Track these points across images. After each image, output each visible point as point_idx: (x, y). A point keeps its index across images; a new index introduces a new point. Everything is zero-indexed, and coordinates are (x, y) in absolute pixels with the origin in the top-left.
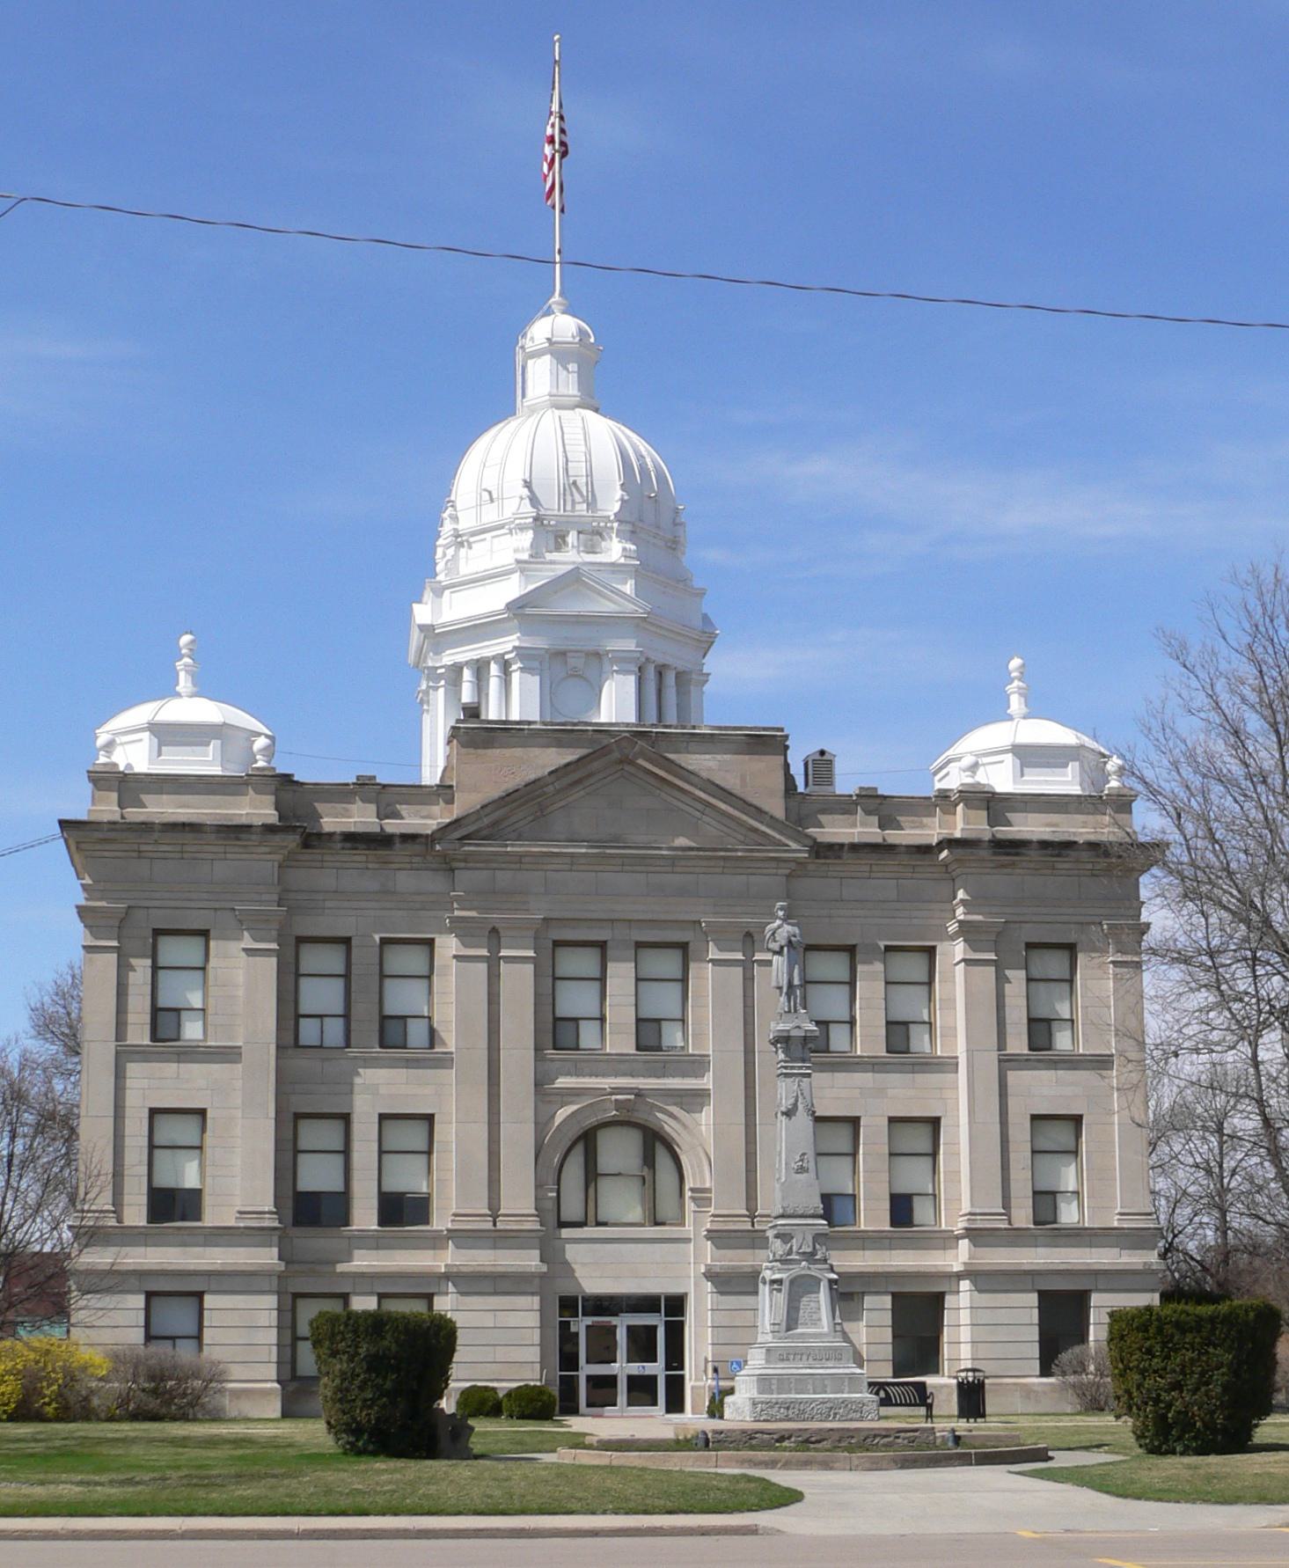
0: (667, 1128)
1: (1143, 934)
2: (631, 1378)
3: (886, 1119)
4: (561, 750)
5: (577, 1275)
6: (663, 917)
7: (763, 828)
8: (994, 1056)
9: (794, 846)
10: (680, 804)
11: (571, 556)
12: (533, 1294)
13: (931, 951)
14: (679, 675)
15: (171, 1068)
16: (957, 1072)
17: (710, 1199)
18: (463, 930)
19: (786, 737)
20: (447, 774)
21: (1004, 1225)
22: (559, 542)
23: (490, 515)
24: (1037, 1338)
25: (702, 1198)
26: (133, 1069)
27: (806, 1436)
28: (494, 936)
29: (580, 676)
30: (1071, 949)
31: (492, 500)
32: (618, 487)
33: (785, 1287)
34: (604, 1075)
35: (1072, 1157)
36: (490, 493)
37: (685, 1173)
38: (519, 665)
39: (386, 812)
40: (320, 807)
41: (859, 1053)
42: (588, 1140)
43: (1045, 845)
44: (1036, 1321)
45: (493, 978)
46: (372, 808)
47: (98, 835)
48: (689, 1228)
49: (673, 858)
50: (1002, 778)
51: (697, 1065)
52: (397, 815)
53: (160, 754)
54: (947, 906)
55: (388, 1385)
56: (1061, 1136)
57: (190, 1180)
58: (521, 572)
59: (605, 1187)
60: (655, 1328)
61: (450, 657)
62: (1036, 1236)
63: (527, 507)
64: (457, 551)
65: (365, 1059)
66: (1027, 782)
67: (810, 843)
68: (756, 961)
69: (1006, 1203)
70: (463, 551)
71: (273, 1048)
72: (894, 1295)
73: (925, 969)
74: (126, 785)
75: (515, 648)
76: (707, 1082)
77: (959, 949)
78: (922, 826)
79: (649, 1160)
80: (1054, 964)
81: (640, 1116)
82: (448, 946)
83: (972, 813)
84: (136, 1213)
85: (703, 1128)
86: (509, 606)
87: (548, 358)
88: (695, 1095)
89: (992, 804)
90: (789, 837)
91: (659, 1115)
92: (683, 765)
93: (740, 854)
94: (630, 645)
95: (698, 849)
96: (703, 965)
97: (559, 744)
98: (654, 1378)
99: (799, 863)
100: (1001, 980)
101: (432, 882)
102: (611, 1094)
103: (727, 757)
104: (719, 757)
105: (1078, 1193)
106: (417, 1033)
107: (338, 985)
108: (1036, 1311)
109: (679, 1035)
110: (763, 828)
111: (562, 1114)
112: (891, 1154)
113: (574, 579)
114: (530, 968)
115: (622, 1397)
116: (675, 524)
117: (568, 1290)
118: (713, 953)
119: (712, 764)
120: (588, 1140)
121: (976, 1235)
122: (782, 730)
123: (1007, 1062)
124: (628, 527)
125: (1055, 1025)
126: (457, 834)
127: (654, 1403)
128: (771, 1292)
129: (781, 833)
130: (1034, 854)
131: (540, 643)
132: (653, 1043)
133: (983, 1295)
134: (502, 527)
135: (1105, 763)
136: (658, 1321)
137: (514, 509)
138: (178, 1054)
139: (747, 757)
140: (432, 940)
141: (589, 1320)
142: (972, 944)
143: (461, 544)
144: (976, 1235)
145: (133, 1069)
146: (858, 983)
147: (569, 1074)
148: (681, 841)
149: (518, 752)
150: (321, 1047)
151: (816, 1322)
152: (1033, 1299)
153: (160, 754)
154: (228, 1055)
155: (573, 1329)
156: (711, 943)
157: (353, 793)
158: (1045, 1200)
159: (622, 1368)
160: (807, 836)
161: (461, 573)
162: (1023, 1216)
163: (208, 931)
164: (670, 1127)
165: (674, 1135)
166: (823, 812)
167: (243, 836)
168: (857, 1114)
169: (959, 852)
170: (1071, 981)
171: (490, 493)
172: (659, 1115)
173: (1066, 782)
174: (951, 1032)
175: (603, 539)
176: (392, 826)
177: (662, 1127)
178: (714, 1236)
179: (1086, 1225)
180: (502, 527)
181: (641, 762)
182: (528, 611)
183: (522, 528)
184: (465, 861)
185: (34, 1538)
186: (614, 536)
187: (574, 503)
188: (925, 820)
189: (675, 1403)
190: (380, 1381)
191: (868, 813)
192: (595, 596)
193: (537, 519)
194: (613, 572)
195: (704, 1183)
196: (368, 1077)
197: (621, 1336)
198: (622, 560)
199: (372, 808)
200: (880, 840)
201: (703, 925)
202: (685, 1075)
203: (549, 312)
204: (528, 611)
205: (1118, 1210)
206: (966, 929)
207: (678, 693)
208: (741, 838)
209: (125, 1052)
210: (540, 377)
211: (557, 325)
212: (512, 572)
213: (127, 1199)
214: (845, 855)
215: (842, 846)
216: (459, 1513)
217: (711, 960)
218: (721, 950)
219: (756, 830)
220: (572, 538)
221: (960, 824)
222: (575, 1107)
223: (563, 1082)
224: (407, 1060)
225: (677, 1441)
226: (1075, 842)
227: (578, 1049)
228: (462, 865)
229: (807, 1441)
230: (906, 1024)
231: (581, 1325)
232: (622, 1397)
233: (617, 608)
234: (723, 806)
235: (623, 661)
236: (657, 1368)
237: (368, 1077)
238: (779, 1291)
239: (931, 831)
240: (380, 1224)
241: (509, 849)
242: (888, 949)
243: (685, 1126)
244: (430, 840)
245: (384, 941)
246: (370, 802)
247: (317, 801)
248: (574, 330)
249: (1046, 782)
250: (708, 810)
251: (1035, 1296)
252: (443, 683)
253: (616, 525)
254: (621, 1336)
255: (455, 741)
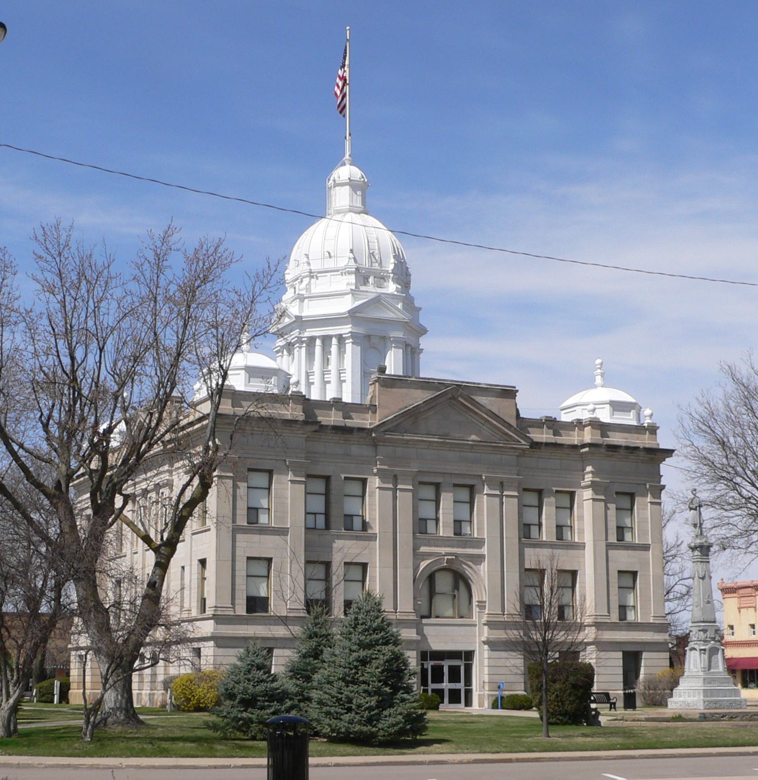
0: (467, 572)
1: (662, 490)
2: (450, 690)
3: (246, 558)
4: (424, 391)
5: (429, 641)
6: (431, 470)
7: (511, 433)
8: (604, 543)
9: (523, 442)
10: (473, 420)
11: (371, 290)
12: (413, 650)
13: (572, 495)
14: (412, 348)
15: (256, 537)
16: (584, 549)
17: (485, 606)
18: (382, 474)
19: (517, 391)
20: (373, 399)
21: (232, 613)
22: (365, 281)
23: (330, 264)
24: (622, 672)
25: (482, 605)
26: (239, 537)
27: (731, 715)
28: (395, 479)
29: (375, 348)
30: (270, 473)
31: (330, 257)
32: (392, 257)
33: (707, 653)
34: (440, 546)
35: (632, 590)
36: (329, 253)
37: (473, 594)
38: (351, 340)
39: (604, 435)
40: (317, 412)
41: (441, 535)
42: (431, 578)
43: (627, 448)
44: (621, 665)
45: (395, 498)
46: (341, 413)
47: (227, 421)
48: (475, 618)
49: (472, 445)
50: (605, 416)
51: (479, 543)
52: (350, 418)
53: (249, 382)
54: (581, 473)
55: (579, 694)
56: (261, 569)
57: (263, 593)
58: (353, 295)
59: (437, 600)
60: (460, 666)
61: (309, 332)
62: (621, 626)
63: (352, 262)
64: (310, 279)
65: (338, 535)
66: (615, 418)
67: (530, 441)
68: (399, 489)
69: (233, 603)
70: (313, 280)
71: (303, 529)
72: (623, 651)
73: (569, 502)
74: (237, 397)
75: (350, 332)
76: (484, 550)
77: (588, 494)
78: (570, 436)
79: (456, 587)
80: (260, 480)
81: (455, 567)
82: (374, 482)
83: (594, 431)
84: (241, 610)
85: (482, 573)
86: (349, 312)
87: (348, 187)
88: (480, 557)
89: (603, 428)
90: (521, 438)
91: (464, 566)
92: (480, 402)
93: (470, 443)
94: (400, 334)
95: (481, 442)
96: (482, 495)
97: (422, 388)
98: (459, 690)
99: (523, 450)
100: (235, 487)
101: (367, 451)
102: (445, 556)
103: (493, 399)
104: (489, 398)
105: (634, 607)
106: (357, 524)
107: (322, 499)
108: (621, 661)
109: (469, 528)
110: (511, 433)
111: (423, 565)
112: (248, 576)
113: (377, 301)
114: (516, 500)
115: (446, 699)
116: (407, 275)
117: (425, 649)
118: (486, 490)
119: (485, 401)
120: (431, 578)
121: (598, 625)
122: (515, 387)
123: (609, 546)
124: (396, 277)
125: (625, 530)
126: (383, 429)
127: (459, 702)
128: (701, 654)
129: (518, 436)
130: (622, 451)
131: (360, 330)
132: (423, 531)
133: (495, 652)
134: (338, 271)
135: (290, 378)
136: (461, 663)
137: (346, 263)
138: (260, 530)
139: (500, 399)
140: (366, 479)
141: (432, 663)
142: (596, 492)
143: (312, 277)
144: (598, 625)
145: (239, 537)
146: (544, 508)
147: (425, 545)
148: (473, 437)
149: (404, 391)
150: (315, 528)
151: (718, 667)
152: (620, 654)
153: (249, 382)
154: (282, 532)
155: (425, 667)
156: (486, 486)
157: (333, 406)
158: (623, 609)
159: (446, 685)
160: (529, 438)
161: (312, 292)
162: (615, 617)
163: (272, 470)
164: (468, 572)
165: (470, 576)
166: (530, 427)
167: (293, 425)
168: (635, 570)
169: (593, 449)
170: (269, 489)
171: (329, 253)
172: (464, 566)
173: (629, 419)
174: (581, 532)
175: (385, 281)
176: (349, 423)
177: (465, 572)
178: (491, 624)
179: (639, 621)
180: (338, 271)
181: (460, 399)
182: (357, 315)
183: (350, 273)
184: (384, 442)
185: (567, 760)
186: (390, 280)
187: (372, 262)
188: (571, 433)
189: (468, 703)
190: (576, 692)
191: (549, 428)
192: (383, 308)
193: (357, 269)
194: (393, 298)
195: (482, 598)
196: (338, 544)
197: (446, 670)
198: (396, 293)
199: (341, 413)
200: (554, 441)
201: (287, 463)
202: (474, 547)
203: (344, 164)
204: (357, 315)
205: (652, 615)
206: (593, 485)
207: (411, 358)
208: (499, 437)
209: (237, 529)
210: (341, 197)
211: (346, 172)
212: (347, 294)
213: (237, 602)
214: (543, 447)
215: (542, 443)
216: (744, 746)
217: (486, 494)
218: (490, 489)
219: (507, 434)
220: (371, 280)
221: (588, 436)
222: (429, 562)
223: (423, 549)
224: (357, 536)
225: (673, 718)
226: (639, 448)
227: (426, 533)
228: (381, 443)
229: (732, 717)
230: (352, 516)
231: (429, 664)
232: (446, 699)
233: (395, 316)
234: (495, 422)
235: (398, 343)
236: (461, 686)
237: (338, 544)
238: (704, 654)
239: (574, 438)
240: (247, 613)
241: (405, 437)
242: (557, 491)
243: (475, 572)
244: (370, 431)
245: (346, 478)
246: (340, 410)
247: (609, 431)
248: (360, 176)
249: (623, 419)
250: (486, 424)
251: (621, 653)
252: (304, 345)
253: (392, 275)
254: (446, 670)
255: (377, 384)
